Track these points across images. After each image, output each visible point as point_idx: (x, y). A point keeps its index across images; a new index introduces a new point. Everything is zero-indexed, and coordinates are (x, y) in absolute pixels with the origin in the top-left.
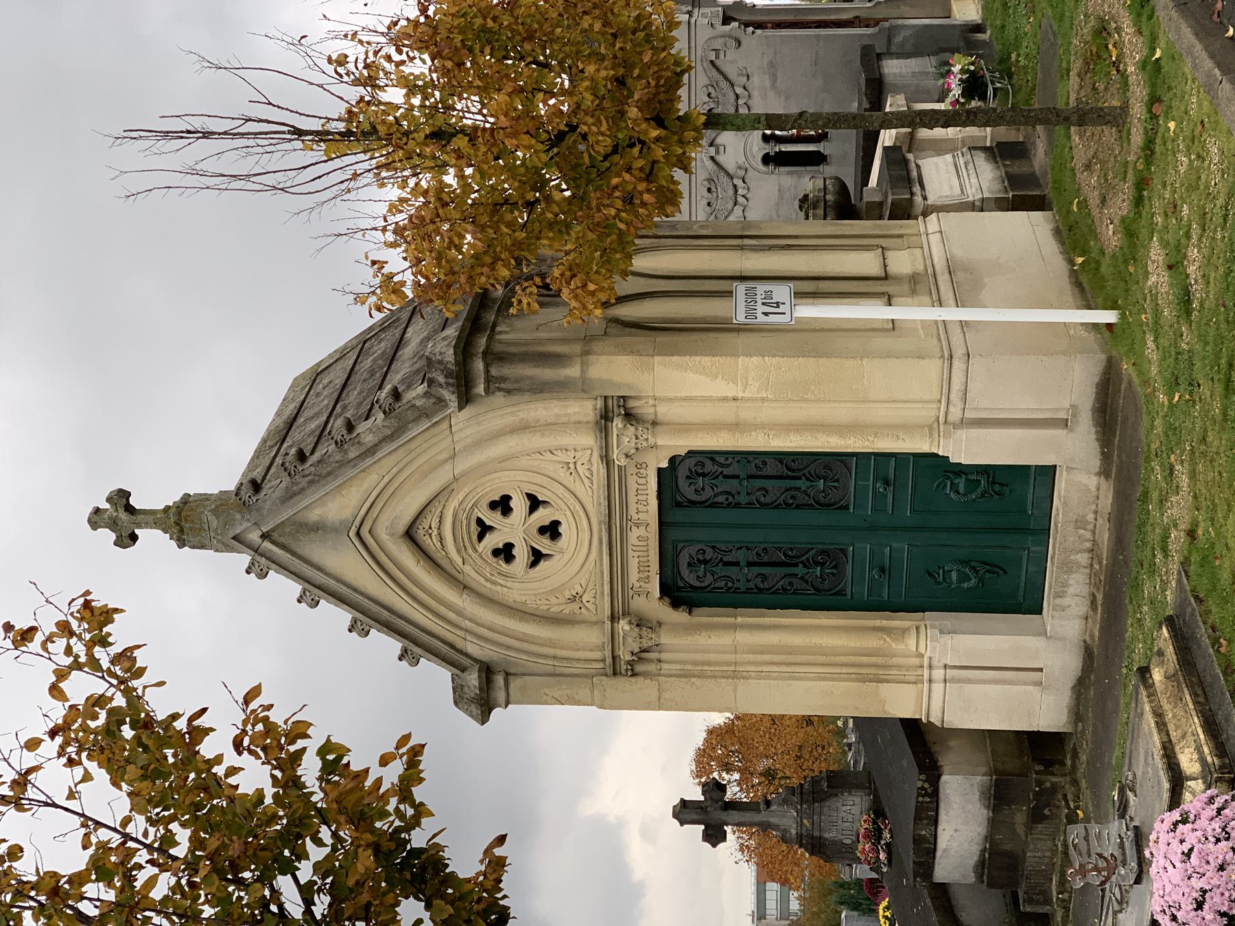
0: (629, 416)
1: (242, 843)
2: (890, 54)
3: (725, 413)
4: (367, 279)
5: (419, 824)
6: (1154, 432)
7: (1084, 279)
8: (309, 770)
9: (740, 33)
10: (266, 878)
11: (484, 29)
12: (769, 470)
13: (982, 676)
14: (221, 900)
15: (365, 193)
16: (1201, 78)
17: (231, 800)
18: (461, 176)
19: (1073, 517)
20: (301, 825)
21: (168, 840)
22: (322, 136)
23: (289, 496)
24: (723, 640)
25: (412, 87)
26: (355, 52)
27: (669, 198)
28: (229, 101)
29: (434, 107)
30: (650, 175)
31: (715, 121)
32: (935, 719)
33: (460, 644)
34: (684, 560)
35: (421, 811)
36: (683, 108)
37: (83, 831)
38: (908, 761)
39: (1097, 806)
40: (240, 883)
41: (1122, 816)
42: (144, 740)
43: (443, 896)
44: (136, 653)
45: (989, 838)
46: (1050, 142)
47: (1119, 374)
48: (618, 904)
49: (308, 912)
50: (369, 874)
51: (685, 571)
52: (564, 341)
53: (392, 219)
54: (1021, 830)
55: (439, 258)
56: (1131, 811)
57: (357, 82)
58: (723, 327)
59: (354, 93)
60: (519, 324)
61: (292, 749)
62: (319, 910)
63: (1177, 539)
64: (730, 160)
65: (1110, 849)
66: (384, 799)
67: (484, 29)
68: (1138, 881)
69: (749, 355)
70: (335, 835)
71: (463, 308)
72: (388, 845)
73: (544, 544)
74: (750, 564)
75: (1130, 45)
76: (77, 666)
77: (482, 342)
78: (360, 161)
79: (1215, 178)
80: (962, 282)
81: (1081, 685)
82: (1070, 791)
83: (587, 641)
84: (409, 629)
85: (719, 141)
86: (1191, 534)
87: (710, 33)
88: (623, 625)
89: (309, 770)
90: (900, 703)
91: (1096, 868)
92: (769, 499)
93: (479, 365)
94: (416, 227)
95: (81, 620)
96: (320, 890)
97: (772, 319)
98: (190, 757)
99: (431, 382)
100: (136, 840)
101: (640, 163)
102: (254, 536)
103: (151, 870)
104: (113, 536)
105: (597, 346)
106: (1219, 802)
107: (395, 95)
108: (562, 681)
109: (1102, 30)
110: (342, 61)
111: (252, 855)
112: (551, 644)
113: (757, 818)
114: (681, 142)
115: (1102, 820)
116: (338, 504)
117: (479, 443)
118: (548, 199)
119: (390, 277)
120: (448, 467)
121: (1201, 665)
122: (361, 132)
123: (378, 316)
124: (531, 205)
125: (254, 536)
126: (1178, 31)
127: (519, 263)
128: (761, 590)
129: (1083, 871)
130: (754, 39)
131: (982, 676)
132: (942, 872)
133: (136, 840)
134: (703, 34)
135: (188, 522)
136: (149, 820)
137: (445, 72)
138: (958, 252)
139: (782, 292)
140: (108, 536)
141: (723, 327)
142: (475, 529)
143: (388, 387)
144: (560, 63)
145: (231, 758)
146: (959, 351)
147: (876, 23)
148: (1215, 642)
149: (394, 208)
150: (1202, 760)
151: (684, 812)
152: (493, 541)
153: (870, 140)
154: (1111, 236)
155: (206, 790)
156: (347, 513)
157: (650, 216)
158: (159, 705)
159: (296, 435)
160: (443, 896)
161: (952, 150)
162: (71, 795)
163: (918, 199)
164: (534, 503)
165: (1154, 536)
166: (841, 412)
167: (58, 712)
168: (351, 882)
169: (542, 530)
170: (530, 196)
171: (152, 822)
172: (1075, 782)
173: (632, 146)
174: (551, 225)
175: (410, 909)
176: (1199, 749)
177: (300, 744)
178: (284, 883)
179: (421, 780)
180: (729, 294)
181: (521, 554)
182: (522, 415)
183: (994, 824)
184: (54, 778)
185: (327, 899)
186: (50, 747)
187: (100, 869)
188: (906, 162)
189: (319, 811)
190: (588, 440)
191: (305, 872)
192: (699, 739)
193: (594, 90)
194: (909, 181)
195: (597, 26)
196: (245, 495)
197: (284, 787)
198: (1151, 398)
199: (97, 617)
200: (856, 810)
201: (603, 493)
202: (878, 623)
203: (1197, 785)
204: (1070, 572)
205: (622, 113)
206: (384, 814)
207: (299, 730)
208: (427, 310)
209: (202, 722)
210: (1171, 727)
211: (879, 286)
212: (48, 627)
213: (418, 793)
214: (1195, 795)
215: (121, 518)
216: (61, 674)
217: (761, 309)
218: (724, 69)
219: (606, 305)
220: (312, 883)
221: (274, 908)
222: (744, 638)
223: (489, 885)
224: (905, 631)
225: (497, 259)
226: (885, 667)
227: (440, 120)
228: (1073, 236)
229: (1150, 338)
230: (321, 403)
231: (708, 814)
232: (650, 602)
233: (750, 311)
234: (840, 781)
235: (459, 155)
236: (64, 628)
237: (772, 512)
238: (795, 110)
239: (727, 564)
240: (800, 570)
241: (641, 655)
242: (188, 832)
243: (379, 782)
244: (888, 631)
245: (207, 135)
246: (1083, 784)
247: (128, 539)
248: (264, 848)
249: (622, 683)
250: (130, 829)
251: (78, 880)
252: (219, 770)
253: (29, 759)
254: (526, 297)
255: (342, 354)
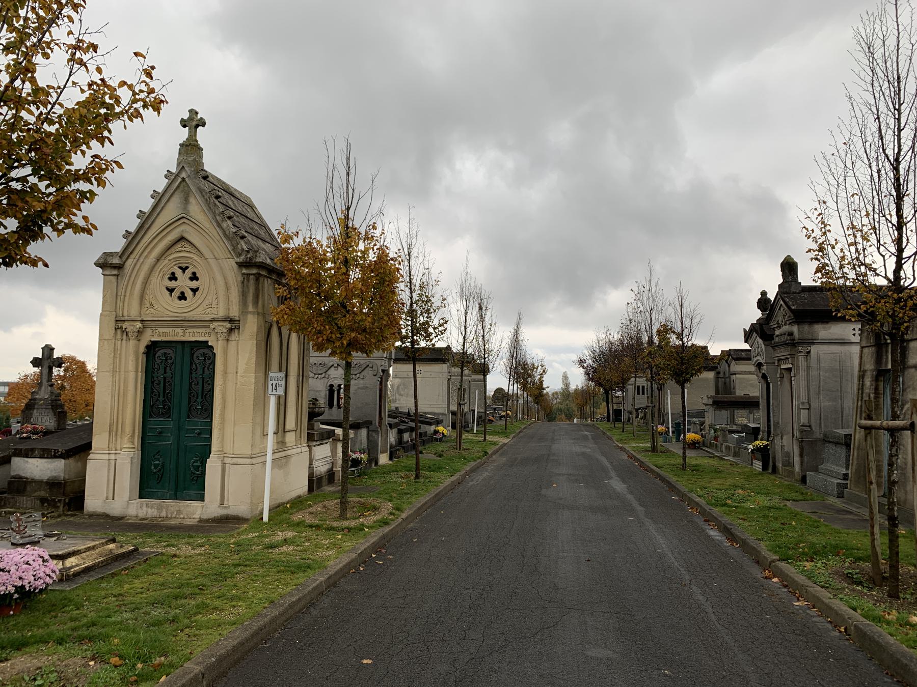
0: (231, 330)
1: (48, 155)
2: (368, 431)
3: (231, 369)
4: (291, 230)
5: (54, 230)
6: (219, 538)
7: (281, 508)
8: (83, 186)
9: (378, 376)
10: (31, 162)
11: (385, 281)
12: (206, 386)
13: (111, 477)
14: (20, 142)
15: (325, 231)
16: (357, 546)
17: (69, 151)
18: (331, 269)
19: (182, 509)
20: (58, 180)
21: (51, 123)
22: (347, 217)
23: (201, 191)
24: (131, 366)
25: (365, 252)
26: (377, 233)
27: (320, 348)
28: (361, 183)
29: (357, 261)
30: (328, 340)
31: (348, 365)
32: (91, 456)
33: (132, 256)
34: (168, 351)
35: (60, 232)
36: (354, 354)
37: (56, 86)
38: (71, 445)
39: (48, 526)
40: (29, 151)
41: (45, 536)
42: (99, 118)
43: (19, 239)
44: (139, 119)
45: (33, 481)
46: (334, 492)
47: (243, 523)
48: (2, 321)
49: (13, 179)
50: (30, 206)
51: (162, 351)
52: (264, 306)
53: (314, 241)
54: (36, 494)
55: (299, 258)
56: (47, 539)
57: (366, 233)
58: (267, 368)
59: (362, 230)
60: (271, 288)
61: (93, 179)
62: (14, 184)
63: (173, 550)
64: (332, 372)
65: (29, 531)
66: (67, 216)
67: (385, 281)
68: (13, 544)
69: (256, 378)
70: (51, 194)
71: (278, 266)
72: (45, 216)
73: (176, 293)
74: (165, 378)
75: (370, 519)
76: (134, 94)
77: (264, 273)
78: (337, 231)
79: (319, 554)
80: (281, 462)
81: (106, 516)
82: (55, 514)
83: (132, 310)
84: (140, 235)
85: (340, 368)
86: (175, 556)
87: (379, 365)
88: (139, 325)
89: (83, 186)
90: (99, 441)
91: (19, 525)
92: (193, 386)
93: (254, 271)
94: (312, 250)
95: (155, 98)
96: (24, 185)
97: (270, 387)
98: (90, 136)
99: (248, 252)
100: (52, 108)
101: (334, 336)
102: (184, 175)
103: (37, 113)
104: (186, 118)
105: (261, 318)
106: (53, 575)
107: (361, 246)
108: (112, 300)
109: (375, 509)
110: (374, 228)
111: (43, 157)
112: (131, 294)
113: (44, 381)
114: (341, 352)
115: (43, 528)
116: (196, 209)
117: (221, 269)
118: (321, 301)
119: (292, 238)
120: (212, 256)
121: (116, 564)
122: (348, 233)
123: (275, 233)
124: (319, 295)
125: (184, 175)
126: (375, 536)
127: (295, 289)
128: (153, 382)
129: (18, 520)
130: (376, 380)
131: (111, 477)
132: (16, 461)
133: (52, 108)
134: (378, 362)
135: (191, 148)
136: (61, 115)
137: (370, 265)
138: (293, 460)
139: (281, 391)
140: (186, 116)
141: (267, 368)
142: (184, 265)
143: (246, 234)
144: (372, 309)
145: (89, 153)
146: (254, 461)
147: (380, 426)
148: (126, 569)
149: (318, 242)
150: (72, 567)
151: (48, 350)
152: (179, 273)
153: (338, 425)
154: (298, 517)
155: (75, 141)
156: (192, 214)
157: (313, 340)
158: (115, 126)
159: (226, 196)
160: (19, 239)
161: (333, 456)
162: (74, 83)
163: (315, 443)
164: (194, 291)
165: (173, 541)
166: (230, 415)
167: (114, 83)
168: (27, 199)
169: (182, 293)
170: (322, 294)
171: (60, 116)
172: (59, 516)
173: (341, 334)
174: (311, 302)
175: (12, 224)
176: (77, 565)
177: (95, 183)
178: (28, 170)
179: (75, 233)
180: (280, 370)
181: (172, 284)
182: (233, 288)
183: (40, 483)
184: (82, 77)
185: (19, 188)
186: (96, 78)
187: (37, 90)
188: (329, 438)
189: (63, 188)
190: (221, 313)
191: (33, 180)
192: (80, 358)
193: (361, 320)
194: (322, 440)
195: (384, 323)
196: (201, 173)
197: (75, 175)
198: (232, 536)
199: (157, 105)
200: (47, 423)
201: (198, 318)
202: (137, 431)
203: (60, 565)
204: (158, 509)
205: (353, 331)
206: (59, 216)
207: (101, 183)
208: (277, 252)
209: (107, 143)
210: (88, 553)
211: (281, 429)
212: (152, 85)
213: (69, 232)
214: (57, 565)
215: (193, 122)
216: (130, 87)
217: (274, 383)
218: (366, 371)
219: (278, 322)
220: (27, 182)
221: (16, 164)
222: (132, 375)
223: (24, 259)
224: (133, 443)
225: (298, 280)
226: (116, 435)
227: (352, 262)
228: (298, 503)
229: (257, 534)
230: (240, 207)
231: (47, 360)
232: (149, 336)
233: (274, 378)
234: (61, 416)
235: (339, 268)
236: (151, 91)
237: (187, 388)
238: (351, 396)
239: (165, 369)
240: (161, 399)
241: (125, 332)
242: (54, 131)
243: (75, 215)
244: (133, 436)
245: (348, 174)
246: (59, 520)
247: (184, 124)
248: (46, 163)
249: (112, 324)
250: (57, 106)
251: (33, 81)
252: (84, 147)
253: (92, 68)
254: (282, 291)
255: (260, 217)
